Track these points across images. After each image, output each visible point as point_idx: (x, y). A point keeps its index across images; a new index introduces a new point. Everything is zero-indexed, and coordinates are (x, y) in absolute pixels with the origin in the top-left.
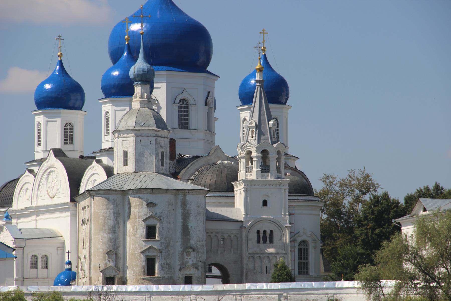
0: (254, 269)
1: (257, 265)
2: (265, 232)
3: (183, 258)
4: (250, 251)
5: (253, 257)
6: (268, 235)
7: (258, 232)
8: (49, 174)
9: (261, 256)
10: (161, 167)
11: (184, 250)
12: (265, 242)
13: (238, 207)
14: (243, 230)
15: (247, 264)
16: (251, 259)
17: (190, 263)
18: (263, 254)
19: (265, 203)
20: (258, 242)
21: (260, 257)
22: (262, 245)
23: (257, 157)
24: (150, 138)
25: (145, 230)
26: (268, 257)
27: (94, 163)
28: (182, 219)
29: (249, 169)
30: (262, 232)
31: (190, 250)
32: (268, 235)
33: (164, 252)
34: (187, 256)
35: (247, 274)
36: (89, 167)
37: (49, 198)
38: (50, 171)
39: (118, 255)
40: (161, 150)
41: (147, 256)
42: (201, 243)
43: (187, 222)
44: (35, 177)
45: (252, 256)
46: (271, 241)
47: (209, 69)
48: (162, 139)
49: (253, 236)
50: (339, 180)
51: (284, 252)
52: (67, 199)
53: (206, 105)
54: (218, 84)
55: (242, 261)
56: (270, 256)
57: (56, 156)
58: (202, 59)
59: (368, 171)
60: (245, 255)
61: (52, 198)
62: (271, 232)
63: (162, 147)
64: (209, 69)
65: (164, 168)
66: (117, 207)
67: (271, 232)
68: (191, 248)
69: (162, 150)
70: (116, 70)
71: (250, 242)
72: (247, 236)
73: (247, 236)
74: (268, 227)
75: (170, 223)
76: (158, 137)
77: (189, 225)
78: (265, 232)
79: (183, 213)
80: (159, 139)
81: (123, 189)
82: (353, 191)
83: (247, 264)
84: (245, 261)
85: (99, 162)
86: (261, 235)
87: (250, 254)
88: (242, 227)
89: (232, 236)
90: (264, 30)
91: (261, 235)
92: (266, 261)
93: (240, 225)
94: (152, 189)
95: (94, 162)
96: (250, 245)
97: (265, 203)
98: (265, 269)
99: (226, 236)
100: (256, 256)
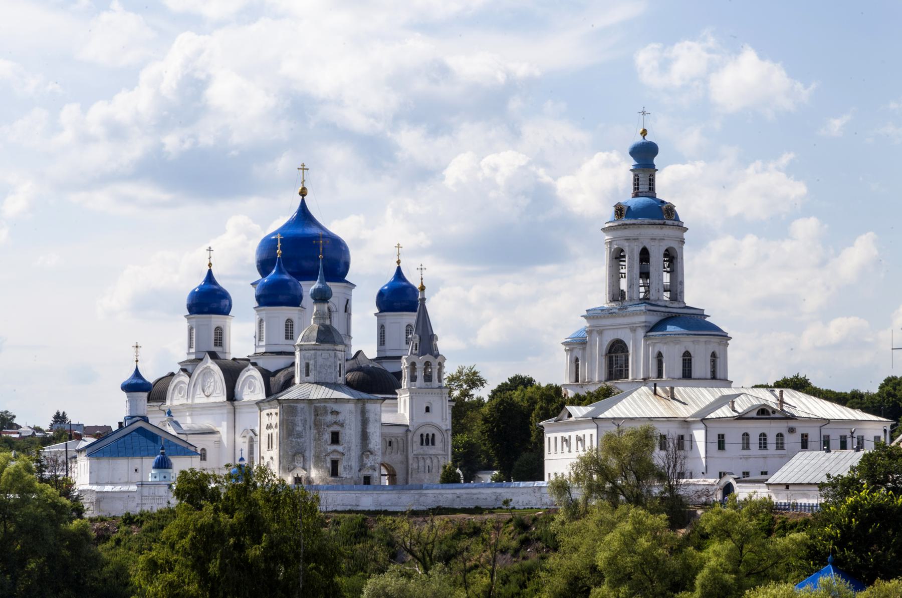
0: (418, 468)
1: (420, 465)
2: (428, 435)
3: (362, 461)
4: (415, 452)
5: (418, 458)
6: (430, 438)
7: (422, 435)
8: (204, 374)
9: (425, 457)
10: (339, 378)
11: (363, 454)
12: (427, 444)
13: (402, 412)
14: (409, 433)
15: (412, 464)
16: (416, 459)
17: (369, 465)
18: (426, 455)
19: (428, 410)
20: (422, 444)
21: (423, 458)
22: (425, 447)
23: (421, 368)
24: (330, 352)
25: (340, 439)
26: (431, 458)
27: (251, 367)
28: (361, 425)
29: (413, 379)
30: (431, 435)
31: (369, 453)
32: (430, 438)
33: (346, 455)
34: (366, 458)
35: (412, 473)
36: (244, 370)
37: (204, 396)
38: (207, 372)
39: (305, 457)
40: (339, 362)
41: (332, 458)
42: (378, 447)
43: (366, 428)
44: (190, 376)
45: (417, 457)
46: (433, 444)
47: (347, 278)
48: (340, 352)
49: (417, 439)
50: (449, 375)
51: (444, 453)
52: (224, 398)
53: (346, 311)
54: (354, 292)
55: (407, 461)
56: (432, 456)
57: (211, 358)
58: (341, 269)
59: (476, 369)
60: (411, 456)
61: (208, 396)
62: (433, 435)
63: (339, 360)
64: (347, 278)
65: (341, 378)
66: (304, 414)
67: (433, 435)
68: (369, 451)
69: (340, 362)
70: (434, 343)
71: (414, 444)
72: (412, 439)
73: (412, 439)
74: (430, 431)
75: (351, 429)
76: (337, 350)
77: (368, 431)
78: (428, 435)
79: (362, 420)
80: (338, 352)
81: (310, 398)
82: (461, 386)
83: (412, 464)
84: (410, 461)
85: (254, 364)
86: (424, 438)
87: (415, 455)
88: (408, 430)
89: (399, 439)
90: (399, 245)
91: (424, 438)
92: (428, 462)
93: (406, 428)
94: (336, 399)
95: (250, 364)
96: (415, 447)
97: (428, 410)
98: (427, 468)
99: (393, 439)
100: (420, 457)
